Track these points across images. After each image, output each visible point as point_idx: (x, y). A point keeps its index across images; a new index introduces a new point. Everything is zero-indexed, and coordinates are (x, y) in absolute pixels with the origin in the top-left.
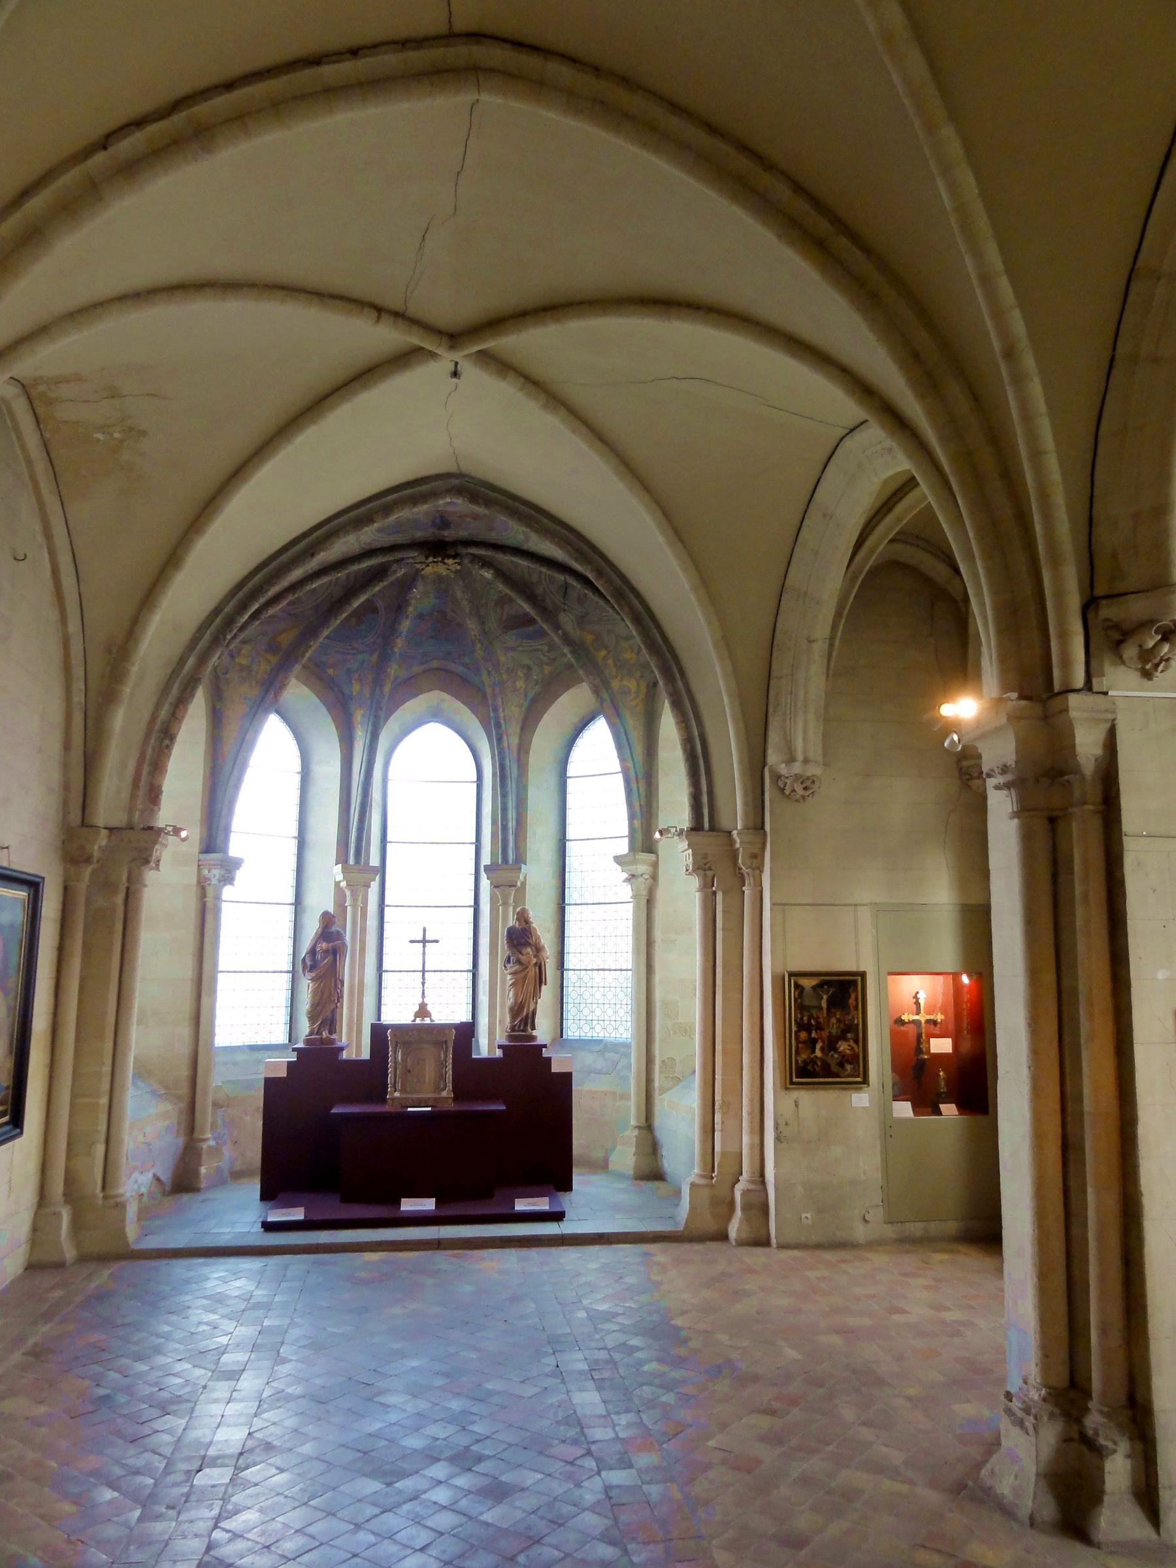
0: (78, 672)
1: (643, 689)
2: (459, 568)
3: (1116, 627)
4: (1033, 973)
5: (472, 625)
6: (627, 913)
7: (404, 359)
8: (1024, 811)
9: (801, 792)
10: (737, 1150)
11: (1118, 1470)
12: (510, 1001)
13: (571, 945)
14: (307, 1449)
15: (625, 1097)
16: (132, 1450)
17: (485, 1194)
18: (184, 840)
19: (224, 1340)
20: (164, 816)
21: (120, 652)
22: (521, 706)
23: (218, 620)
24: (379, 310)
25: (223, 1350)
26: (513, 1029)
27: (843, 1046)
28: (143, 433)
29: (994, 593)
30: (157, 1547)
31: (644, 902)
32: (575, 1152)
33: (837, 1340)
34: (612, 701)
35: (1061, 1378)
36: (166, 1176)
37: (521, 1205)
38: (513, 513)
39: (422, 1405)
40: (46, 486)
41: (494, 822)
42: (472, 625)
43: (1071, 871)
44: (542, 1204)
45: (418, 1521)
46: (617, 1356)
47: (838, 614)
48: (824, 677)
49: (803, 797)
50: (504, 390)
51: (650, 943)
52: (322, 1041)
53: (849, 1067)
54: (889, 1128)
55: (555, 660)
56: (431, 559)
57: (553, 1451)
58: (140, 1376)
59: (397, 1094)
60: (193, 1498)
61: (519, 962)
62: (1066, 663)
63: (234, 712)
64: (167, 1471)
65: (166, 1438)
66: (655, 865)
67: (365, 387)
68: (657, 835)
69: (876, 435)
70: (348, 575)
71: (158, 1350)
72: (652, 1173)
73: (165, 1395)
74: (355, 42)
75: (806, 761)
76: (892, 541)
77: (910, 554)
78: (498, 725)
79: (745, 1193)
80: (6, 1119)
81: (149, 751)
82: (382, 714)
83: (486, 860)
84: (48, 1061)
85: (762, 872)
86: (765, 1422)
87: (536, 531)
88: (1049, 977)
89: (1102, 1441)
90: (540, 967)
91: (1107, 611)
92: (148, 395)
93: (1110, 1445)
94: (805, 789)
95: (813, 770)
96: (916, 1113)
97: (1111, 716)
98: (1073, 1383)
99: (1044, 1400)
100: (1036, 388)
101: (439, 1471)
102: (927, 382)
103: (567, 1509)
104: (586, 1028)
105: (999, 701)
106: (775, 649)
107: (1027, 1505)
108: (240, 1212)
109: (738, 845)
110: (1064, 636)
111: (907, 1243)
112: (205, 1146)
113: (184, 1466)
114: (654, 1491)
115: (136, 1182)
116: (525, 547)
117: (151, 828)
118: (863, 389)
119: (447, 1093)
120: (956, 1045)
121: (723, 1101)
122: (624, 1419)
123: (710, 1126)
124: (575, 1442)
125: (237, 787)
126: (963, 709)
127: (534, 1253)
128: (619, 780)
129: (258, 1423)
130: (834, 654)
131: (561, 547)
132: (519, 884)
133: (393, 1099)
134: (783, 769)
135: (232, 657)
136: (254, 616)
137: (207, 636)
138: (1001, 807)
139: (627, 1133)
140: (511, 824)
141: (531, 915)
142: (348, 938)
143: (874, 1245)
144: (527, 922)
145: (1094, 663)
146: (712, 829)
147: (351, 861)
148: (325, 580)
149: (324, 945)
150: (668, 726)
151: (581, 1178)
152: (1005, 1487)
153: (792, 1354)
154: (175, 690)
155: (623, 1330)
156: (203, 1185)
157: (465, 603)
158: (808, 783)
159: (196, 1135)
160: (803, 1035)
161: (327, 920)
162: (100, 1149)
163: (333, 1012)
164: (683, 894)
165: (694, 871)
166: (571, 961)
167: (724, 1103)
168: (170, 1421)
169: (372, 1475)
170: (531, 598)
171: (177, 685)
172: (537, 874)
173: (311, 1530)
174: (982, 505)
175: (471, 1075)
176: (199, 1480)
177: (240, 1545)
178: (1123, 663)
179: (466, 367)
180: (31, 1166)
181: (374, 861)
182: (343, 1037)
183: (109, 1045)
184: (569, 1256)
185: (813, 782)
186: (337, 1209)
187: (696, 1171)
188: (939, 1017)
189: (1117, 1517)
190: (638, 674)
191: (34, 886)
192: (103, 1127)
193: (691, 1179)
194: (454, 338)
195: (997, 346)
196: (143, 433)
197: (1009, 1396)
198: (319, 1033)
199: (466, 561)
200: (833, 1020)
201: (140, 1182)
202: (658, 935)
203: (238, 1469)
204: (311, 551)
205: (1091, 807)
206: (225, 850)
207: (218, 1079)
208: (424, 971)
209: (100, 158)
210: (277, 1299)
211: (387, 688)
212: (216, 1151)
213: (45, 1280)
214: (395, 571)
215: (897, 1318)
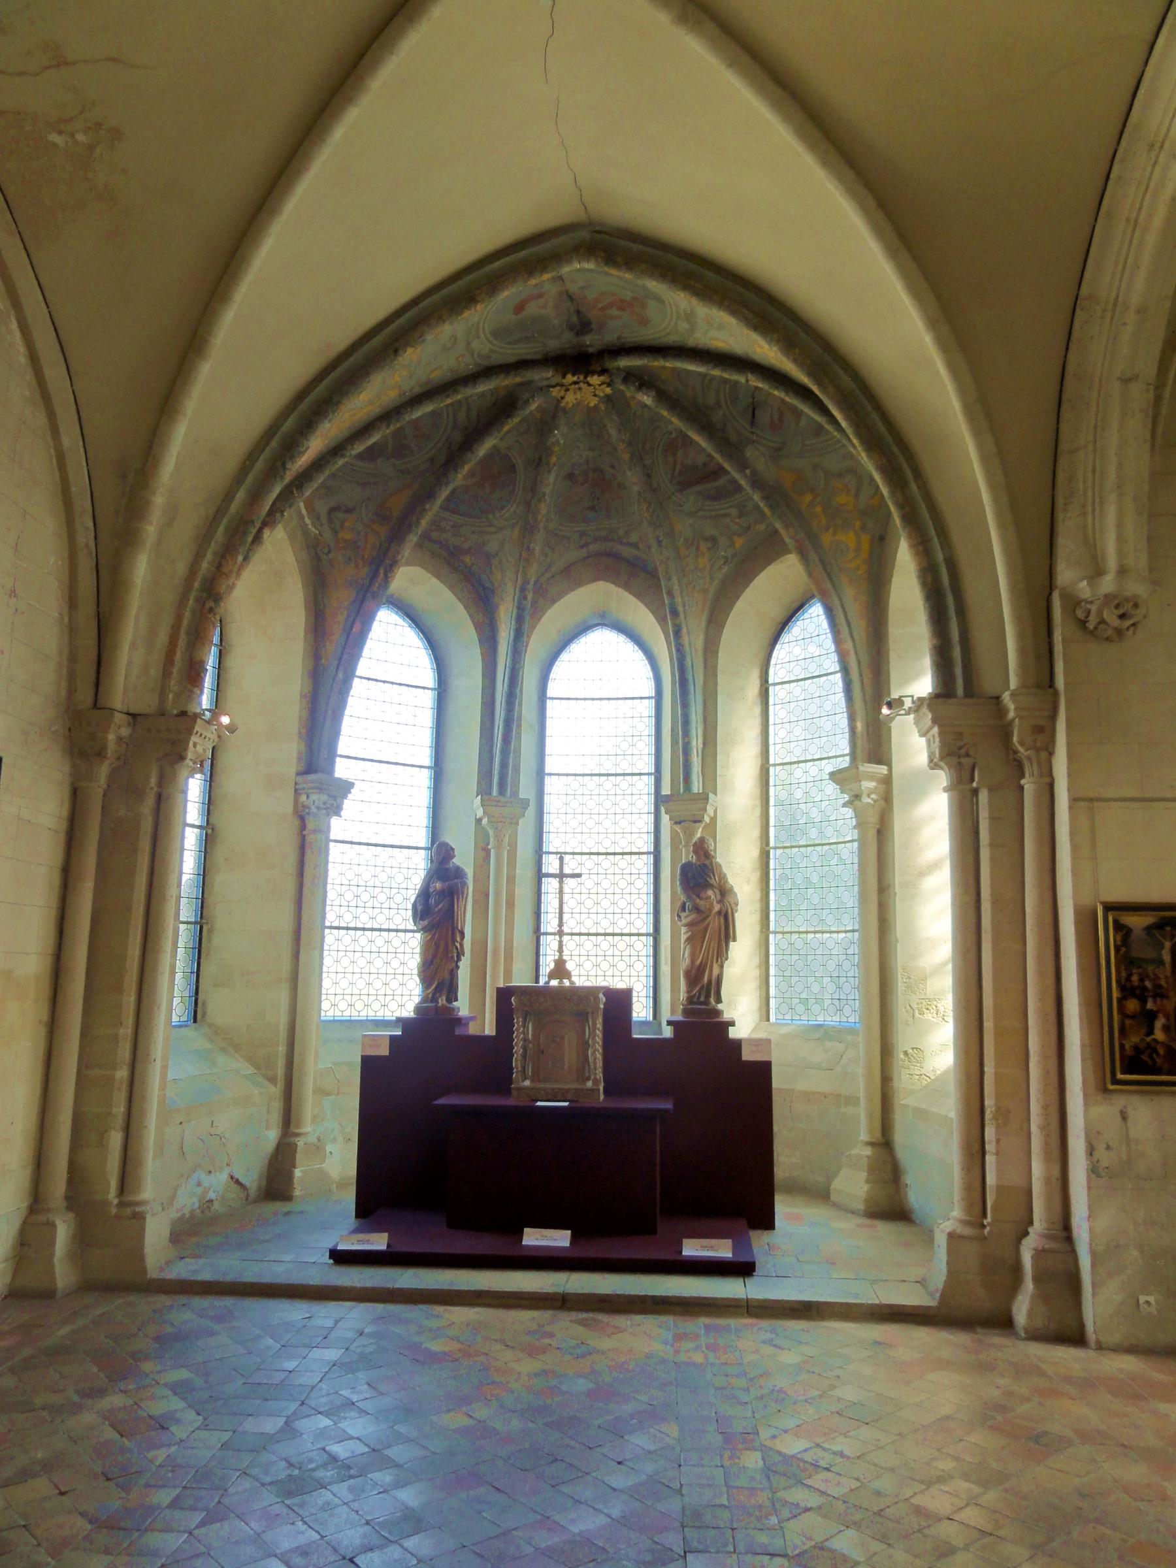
0: (83, 503)
1: (866, 545)
2: (608, 390)
5: (633, 479)
6: (849, 853)
9: (1116, 622)
12: (685, 964)
17: (643, 1226)
22: (705, 592)
23: (274, 443)
26: (690, 1000)
31: (872, 834)
34: (822, 562)
37: (692, 1249)
41: (674, 743)
48: (1147, 446)
49: (1119, 632)
52: (437, 1009)
55: (748, 528)
59: (527, 1083)
61: (697, 909)
63: (341, 598)
72: (892, 1208)
75: (1122, 571)
78: (675, 613)
79: (1039, 1254)
81: (187, 615)
84: (45, 1016)
85: (1051, 754)
92: (108, 59)
94: (1122, 617)
95: (1136, 588)
106: (1064, 406)
109: (1011, 714)
115: (199, 1184)
116: (691, 343)
121: (998, 1108)
123: (977, 1146)
130: (1164, 410)
132: (707, 819)
133: (520, 1089)
134: (1084, 589)
135: (335, 532)
137: (260, 465)
139: (855, 1152)
146: (969, 692)
147: (495, 792)
148: (428, 408)
149: (438, 885)
151: (789, 1210)
156: (297, 1192)
157: (622, 446)
159: (294, 1129)
160: (1132, 1005)
162: (115, 1139)
164: (930, 822)
165: (942, 758)
167: (1003, 1114)
171: (221, 529)
181: (526, 790)
182: (463, 1006)
183: (130, 999)
185: (1136, 606)
187: (957, 1213)
190: (858, 524)
192: (120, 1110)
196: (116, 134)
198: (434, 999)
201: (206, 1184)
214: (527, 402)
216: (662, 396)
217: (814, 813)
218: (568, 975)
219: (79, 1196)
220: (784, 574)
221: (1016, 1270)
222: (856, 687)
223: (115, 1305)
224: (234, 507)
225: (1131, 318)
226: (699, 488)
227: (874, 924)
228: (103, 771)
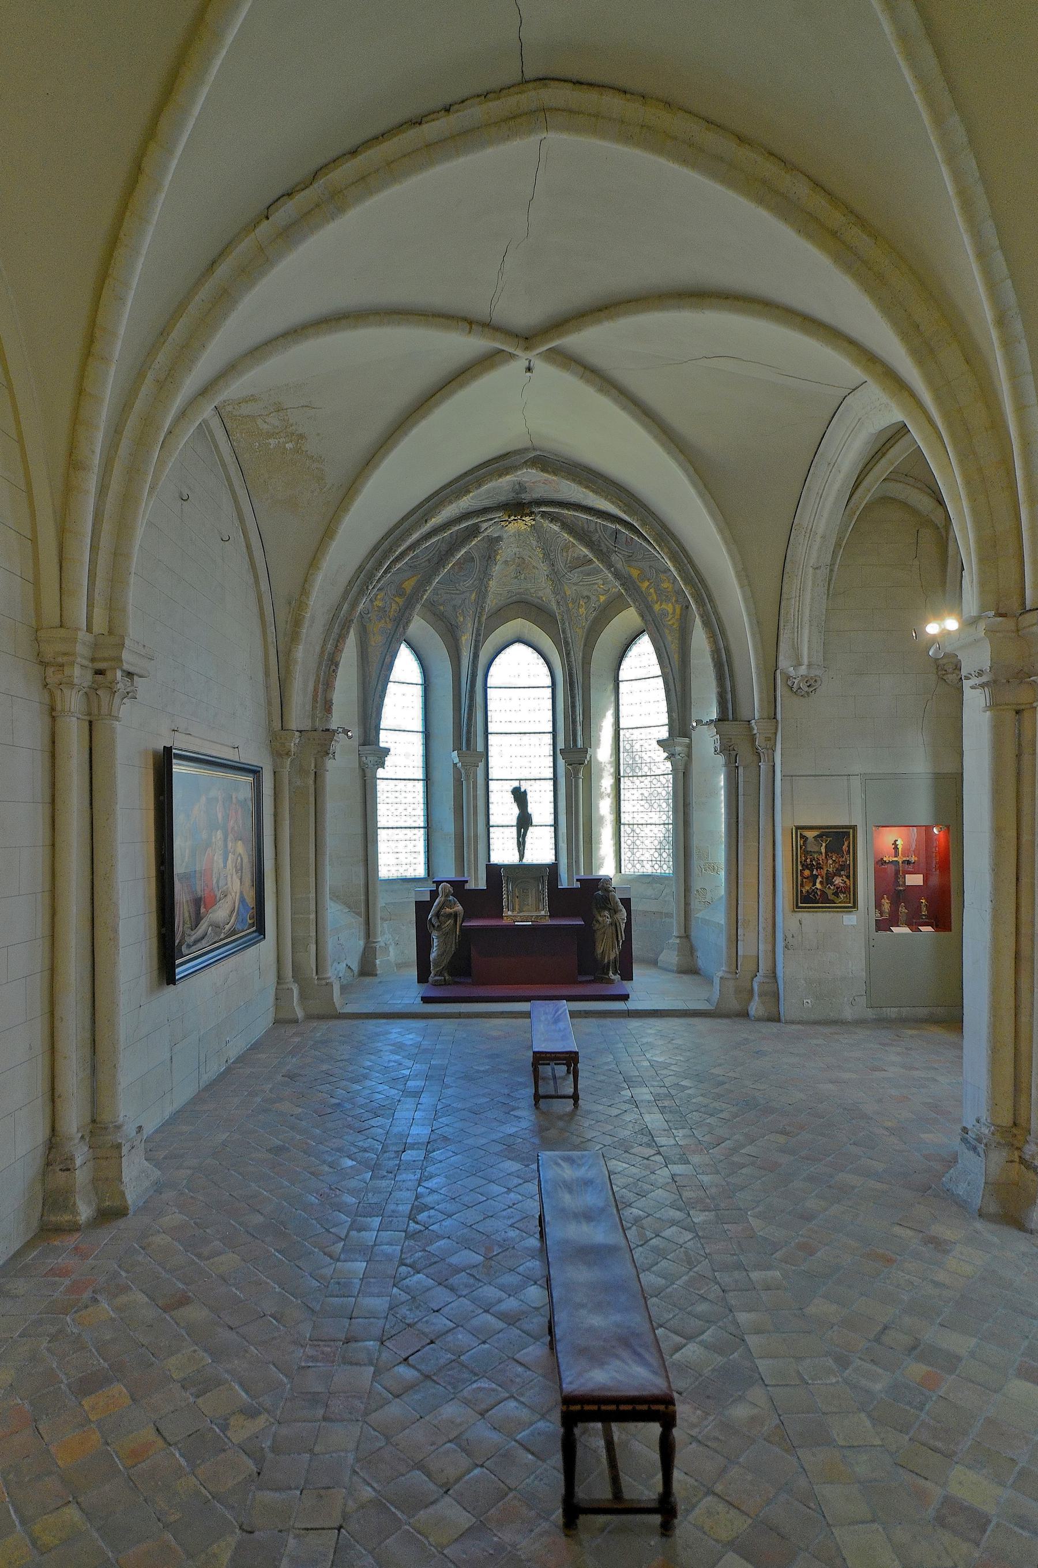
1: (678, 611)
4: (998, 832)
7: (488, 361)
8: (994, 705)
9: (807, 689)
16: (361, 1137)
19: (407, 1072)
25: (407, 1078)
27: (837, 881)
35: (1006, 1120)
49: (807, 693)
53: (842, 896)
56: (513, 518)
57: (633, 1151)
59: (510, 913)
60: (402, 1167)
64: (384, 1151)
66: (689, 746)
67: (462, 386)
74: (448, 100)
75: (809, 666)
77: (897, 490)
83: (561, 745)
86: (782, 1139)
95: (815, 672)
102: (923, 352)
103: (646, 1187)
104: (638, 866)
107: (977, 1202)
109: (755, 732)
111: (882, 1022)
113: (395, 1148)
117: (327, 730)
120: (925, 880)
122: (680, 1133)
124: (649, 1145)
126: (942, 626)
127: (608, 1022)
129: (436, 1125)
131: (613, 503)
136: (385, 572)
138: (975, 703)
140: (579, 718)
143: (860, 1022)
152: (961, 1190)
154: (336, 629)
160: (807, 873)
170: (590, 544)
174: (967, 454)
176: (404, 1156)
177: (435, 1197)
179: (539, 365)
181: (480, 748)
184: (634, 1024)
188: (913, 859)
191: (255, 772)
193: (720, 974)
194: (528, 339)
197: (965, 1130)
199: (538, 518)
200: (830, 862)
203: (428, 1152)
209: (265, 225)
210: (437, 1047)
215: (878, 1074)
217: (646, 757)
221: (751, 991)
222: (673, 692)
223: (324, 1025)
225: (818, 539)
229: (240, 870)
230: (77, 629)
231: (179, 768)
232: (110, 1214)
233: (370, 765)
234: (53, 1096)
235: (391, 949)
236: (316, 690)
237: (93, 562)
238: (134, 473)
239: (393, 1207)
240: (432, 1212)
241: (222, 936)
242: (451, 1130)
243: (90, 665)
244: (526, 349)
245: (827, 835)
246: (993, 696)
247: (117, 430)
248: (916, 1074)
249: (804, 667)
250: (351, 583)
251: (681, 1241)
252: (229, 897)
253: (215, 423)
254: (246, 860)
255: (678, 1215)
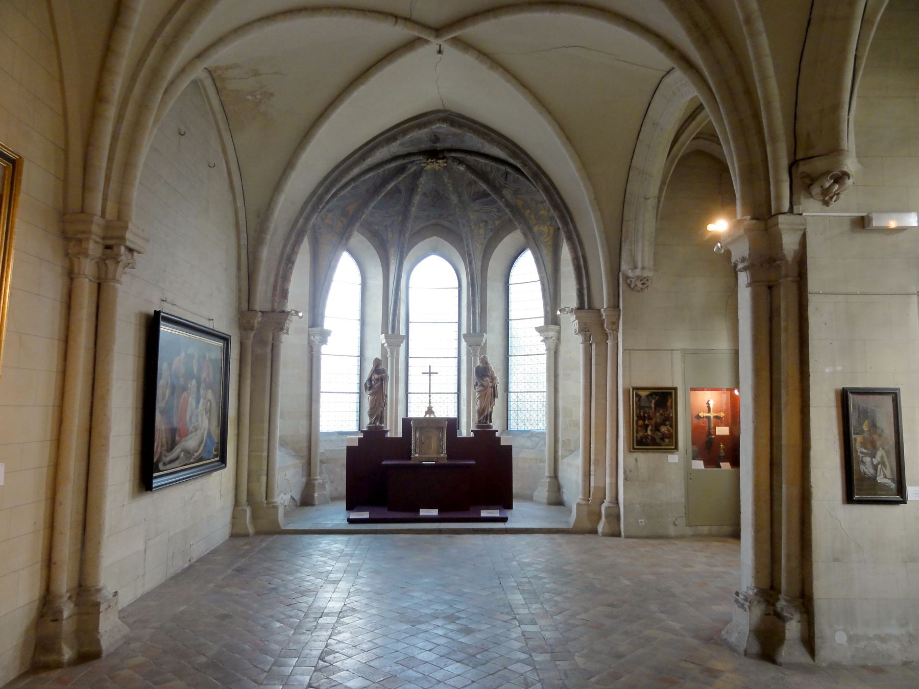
1: (552, 232)
3: (809, 176)
4: (757, 371)
5: (454, 198)
6: (543, 359)
7: (410, 45)
8: (753, 283)
10: (603, 485)
11: (793, 628)
12: (477, 407)
13: (513, 378)
14: (374, 611)
15: (543, 461)
16: (289, 609)
17: (466, 509)
18: (301, 318)
19: (330, 568)
20: (290, 306)
21: (264, 215)
23: (314, 199)
24: (396, 17)
26: (479, 422)
28: (272, 94)
29: (739, 161)
30: (303, 645)
31: (553, 353)
32: (514, 491)
33: (652, 577)
35: (766, 584)
36: (297, 497)
37: (484, 514)
38: (476, 132)
39: (430, 597)
40: (223, 126)
42: (454, 198)
43: (779, 316)
44: (495, 513)
45: (427, 640)
46: (533, 581)
47: (663, 182)
49: (642, 289)
50: (469, 59)
51: (556, 376)
52: (376, 427)
53: (667, 440)
54: (689, 474)
58: (290, 581)
60: (318, 627)
61: (482, 385)
62: (779, 198)
65: (304, 605)
66: (559, 332)
68: (558, 313)
69: (679, 75)
70: (384, 172)
71: (298, 571)
72: (557, 501)
73: (302, 588)
75: (643, 268)
76: (694, 139)
77: (704, 145)
78: (470, 255)
79: (607, 508)
80: (218, 459)
82: (405, 250)
83: (464, 331)
87: (488, 142)
88: (766, 374)
89: (786, 614)
90: (494, 388)
91: (803, 168)
93: (789, 615)
95: (647, 274)
96: (706, 465)
97: (803, 227)
98: (772, 588)
99: (756, 594)
100: (764, 40)
101: (439, 622)
102: (703, 39)
104: (521, 424)
105: (739, 222)
107: (744, 645)
108: (337, 514)
110: (778, 182)
111: (697, 537)
112: (316, 483)
114: (548, 634)
116: (482, 151)
117: (284, 311)
118: (669, 47)
119: (444, 455)
124: (508, 614)
125: (327, 292)
126: (720, 226)
128: (538, 285)
129: (348, 601)
130: (661, 206)
135: (323, 220)
141: (489, 361)
142: (389, 373)
144: (487, 363)
145: (795, 197)
146: (590, 308)
147: (390, 332)
148: (371, 174)
149: (376, 376)
150: (566, 253)
152: (733, 639)
153: (628, 583)
154: (293, 237)
155: (537, 570)
156: (316, 503)
158: (644, 281)
160: (641, 422)
161: (377, 362)
162: (264, 478)
163: (382, 412)
166: (512, 387)
167: (596, 460)
168: (305, 599)
169: (407, 622)
170: (487, 181)
172: (492, 338)
173: (375, 641)
174: (734, 109)
175: (456, 445)
176: (320, 621)
177: (341, 645)
178: (812, 197)
179: (446, 48)
180: (231, 484)
181: (402, 332)
184: (510, 538)
186: (385, 513)
187: (580, 496)
188: (722, 415)
189: (791, 649)
191: (226, 339)
193: (578, 501)
194: (438, 31)
195: (741, 18)
196: (272, 94)
197: (737, 594)
199: (450, 161)
202: (561, 372)
204: (363, 158)
205: (790, 279)
206: (322, 326)
207: (322, 448)
208: (430, 393)
211: (407, 235)
212: (323, 486)
213: (240, 542)
216: (468, 167)
218: (432, 413)
219: (251, 499)
220: (514, 238)
224: (299, 225)
226: (481, 200)
227: (553, 390)
228: (252, 334)
229: (208, 411)
230: (95, 215)
231: (165, 329)
232: (89, 654)
233: (317, 342)
234: (49, 563)
235: (327, 486)
236: (276, 282)
237: (109, 169)
238: (143, 107)
239: (307, 651)
240: (337, 655)
241: (192, 460)
242: (359, 604)
243: (101, 241)
244: (437, 36)
245: (656, 394)
246: (752, 276)
247: (133, 78)
248: (716, 569)
249: (639, 270)
250: (306, 203)
251: (522, 672)
252: (199, 433)
253: (208, 83)
254: (214, 405)
255: (523, 656)
